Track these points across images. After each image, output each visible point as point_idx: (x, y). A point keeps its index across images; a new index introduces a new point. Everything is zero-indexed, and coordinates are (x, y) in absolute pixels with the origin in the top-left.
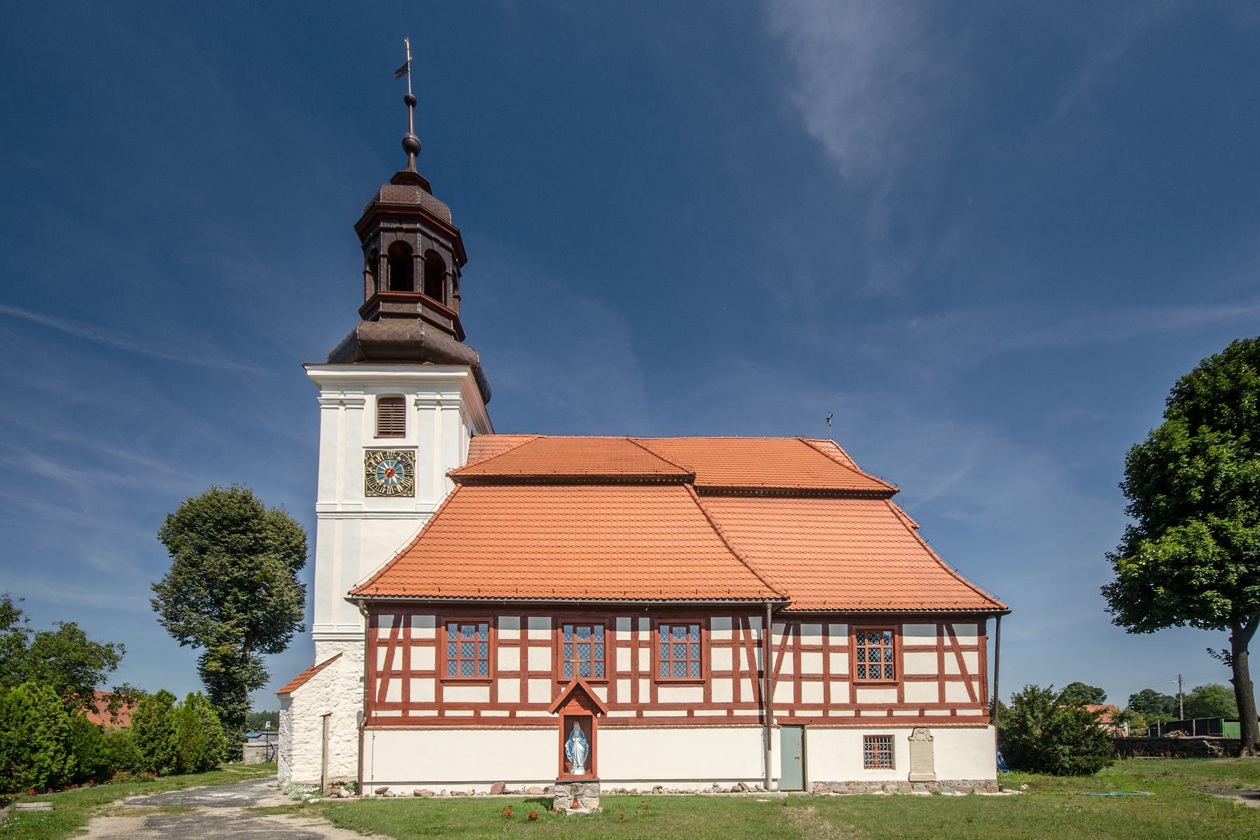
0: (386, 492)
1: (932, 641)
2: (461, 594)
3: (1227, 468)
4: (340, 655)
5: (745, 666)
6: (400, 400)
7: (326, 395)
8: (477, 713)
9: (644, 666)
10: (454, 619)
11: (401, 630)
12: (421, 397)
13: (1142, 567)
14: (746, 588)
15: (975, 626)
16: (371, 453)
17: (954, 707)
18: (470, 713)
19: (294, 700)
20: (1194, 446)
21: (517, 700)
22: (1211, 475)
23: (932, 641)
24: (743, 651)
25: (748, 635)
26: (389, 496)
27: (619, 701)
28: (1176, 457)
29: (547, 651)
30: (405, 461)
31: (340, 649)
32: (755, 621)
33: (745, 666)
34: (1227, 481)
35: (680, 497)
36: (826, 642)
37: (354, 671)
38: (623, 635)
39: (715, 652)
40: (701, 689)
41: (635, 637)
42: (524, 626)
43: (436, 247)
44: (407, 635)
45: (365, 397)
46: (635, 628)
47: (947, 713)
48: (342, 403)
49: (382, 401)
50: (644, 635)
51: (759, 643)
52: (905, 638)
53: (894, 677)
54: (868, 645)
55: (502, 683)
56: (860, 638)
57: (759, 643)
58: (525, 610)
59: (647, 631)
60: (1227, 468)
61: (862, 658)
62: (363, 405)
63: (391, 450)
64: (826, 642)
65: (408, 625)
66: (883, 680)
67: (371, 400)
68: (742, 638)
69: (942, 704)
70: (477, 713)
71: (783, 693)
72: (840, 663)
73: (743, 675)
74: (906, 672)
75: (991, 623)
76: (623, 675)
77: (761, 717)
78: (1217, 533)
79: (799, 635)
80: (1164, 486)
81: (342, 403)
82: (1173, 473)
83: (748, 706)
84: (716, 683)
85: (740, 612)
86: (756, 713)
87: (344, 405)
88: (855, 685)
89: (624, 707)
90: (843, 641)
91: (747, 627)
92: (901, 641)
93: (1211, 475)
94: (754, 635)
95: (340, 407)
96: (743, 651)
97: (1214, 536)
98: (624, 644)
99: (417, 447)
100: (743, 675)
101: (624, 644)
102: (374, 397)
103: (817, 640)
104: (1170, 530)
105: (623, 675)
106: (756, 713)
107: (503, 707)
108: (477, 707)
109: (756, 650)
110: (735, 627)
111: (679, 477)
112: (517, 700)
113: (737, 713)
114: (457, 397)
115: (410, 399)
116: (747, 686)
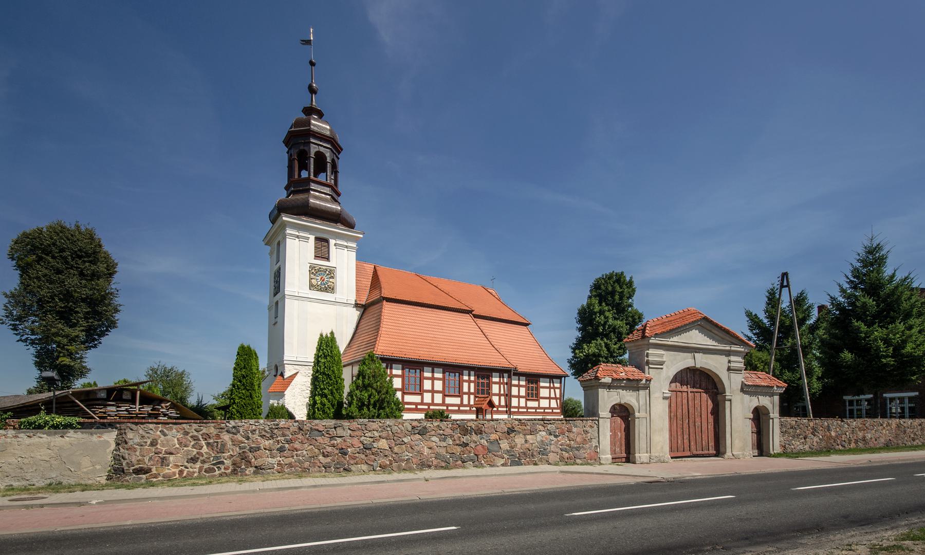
0: (321, 289)
1: (547, 385)
2: (413, 357)
3: (611, 321)
4: (298, 372)
5: (502, 392)
6: (327, 241)
7: (289, 231)
8: (416, 406)
9: (472, 390)
10: (408, 367)
11: (389, 370)
12: (338, 242)
13: (584, 355)
14: (504, 364)
15: (559, 380)
16: (312, 267)
17: (553, 409)
18: (414, 407)
19: (286, 396)
20: (600, 310)
21: (430, 402)
22: (605, 323)
23: (547, 385)
24: (502, 386)
25: (503, 380)
26: (322, 291)
27: (464, 403)
28: (595, 313)
29: (400, 380)
30: (331, 273)
31: (297, 369)
32: (506, 375)
33: (502, 392)
34: (610, 326)
35: (467, 318)
36: (433, 375)
37: (305, 381)
38: (466, 378)
39: (425, 381)
40: (460, 399)
41: (469, 378)
42: (433, 372)
43: (322, 149)
44: (391, 372)
45: (309, 236)
46: (469, 375)
47: (551, 411)
48: (298, 237)
49: (317, 239)
50: (472, 378)
51: (507, 384)
52: (425, 373)
53: (537, 398)
54: (481, 381)
55: (425, 394)
56: (478, 377)
57: (507, 384)
58: (434, 365)
59: (441, 373)
60: (611, 321)
61: (478, 386)
62: (308, 240)
63: (324, 267)
64: (433, 375)
65: (391, 368)
66: (535, 398)
67: (312, 238)
68: (502, 381)
69: (549, 408)
70: (416, 406)
71: (514, 402)
72: (439, 385)
73: (502, 395)
74: (541, 396)
75: (563, 378)
76: (465, 393)
77: (507, 411)
78: (607, 345)
79: (392, 369)
80: (591, 324)
81: (298, 237)
82: (594, 319)
83: (502, 407)
84: (425, 394)
85: (502, 371)
86: (505, 409)
87: (299, 238)
88: (527, 400)
89: (465, 406)
90: (440, 375)
91: (503, 377)
92: (423, 374)
93: (605, 323)
94: (505, 380)
95: (296, 239)
96: (502, 386)
97: (605, 347)
98: (466, 381)
99: (335, 268)
100: (502, 395)
101: (466, 381)
102: (314, 236)
103: (429, 375)
104: (593, 341)
105: (465, 393)
106: (505, 409)
107: (426, 404)
108: (416, 404)
109: (506, 386)
110: (500, 377)
111: (468, 310)
112: (430, 402)
113: (461, 408)
114: (355, 246)
115: (332, 242)
116: (503, 398)
